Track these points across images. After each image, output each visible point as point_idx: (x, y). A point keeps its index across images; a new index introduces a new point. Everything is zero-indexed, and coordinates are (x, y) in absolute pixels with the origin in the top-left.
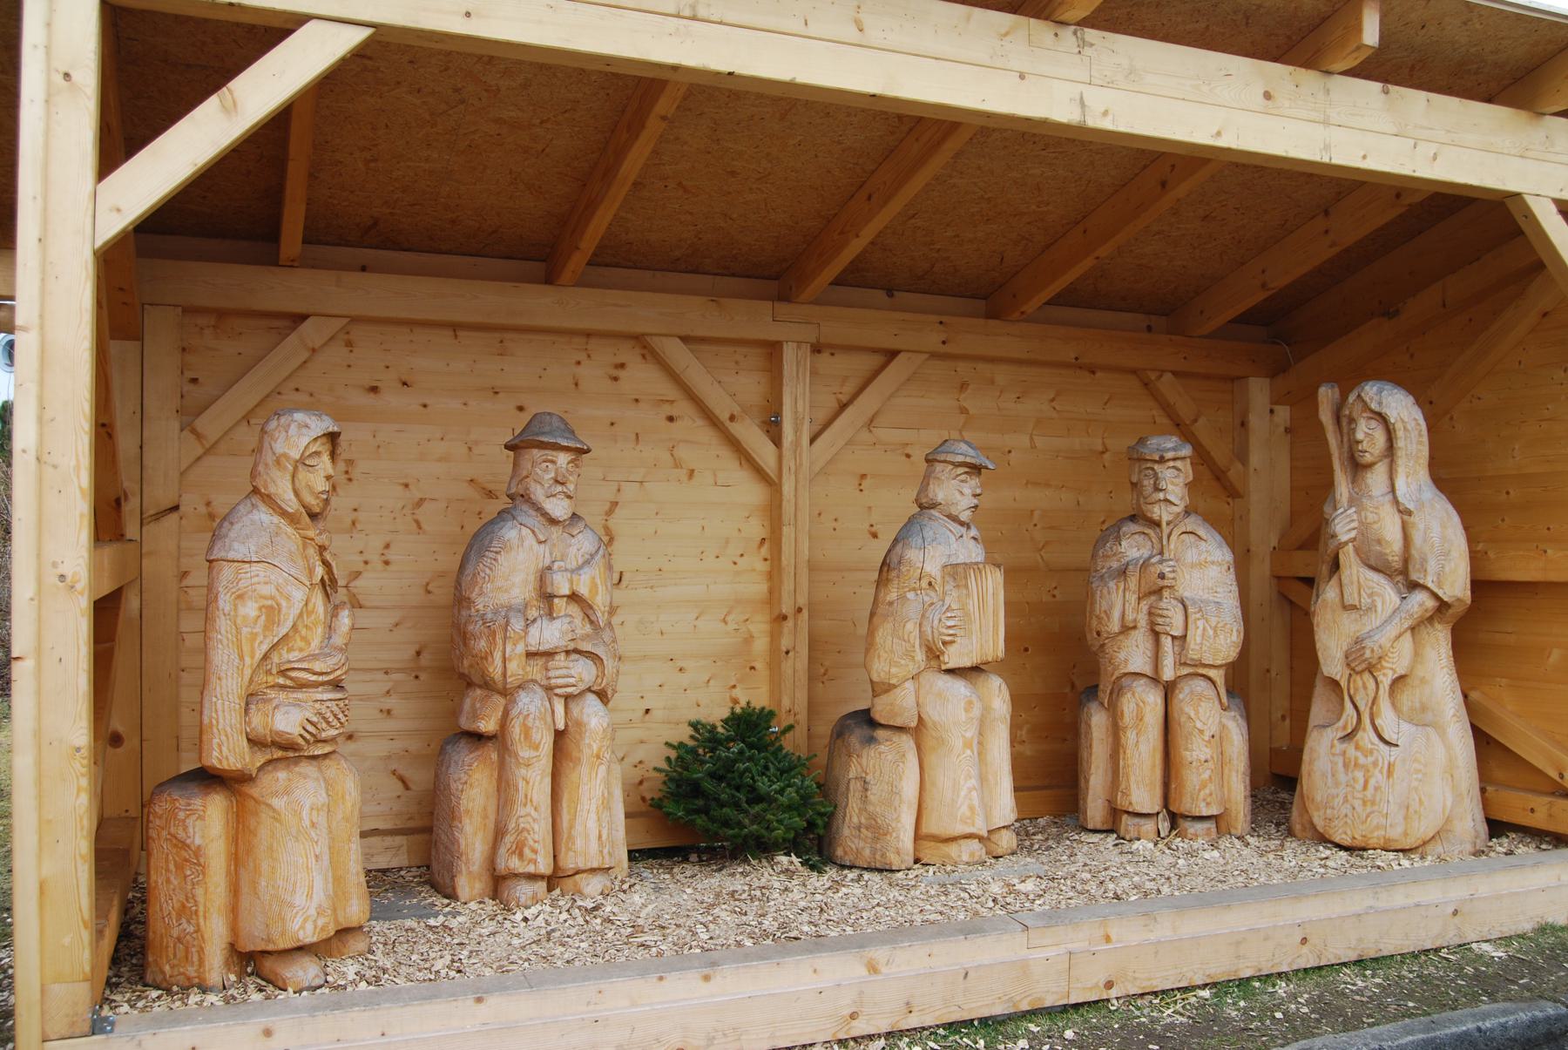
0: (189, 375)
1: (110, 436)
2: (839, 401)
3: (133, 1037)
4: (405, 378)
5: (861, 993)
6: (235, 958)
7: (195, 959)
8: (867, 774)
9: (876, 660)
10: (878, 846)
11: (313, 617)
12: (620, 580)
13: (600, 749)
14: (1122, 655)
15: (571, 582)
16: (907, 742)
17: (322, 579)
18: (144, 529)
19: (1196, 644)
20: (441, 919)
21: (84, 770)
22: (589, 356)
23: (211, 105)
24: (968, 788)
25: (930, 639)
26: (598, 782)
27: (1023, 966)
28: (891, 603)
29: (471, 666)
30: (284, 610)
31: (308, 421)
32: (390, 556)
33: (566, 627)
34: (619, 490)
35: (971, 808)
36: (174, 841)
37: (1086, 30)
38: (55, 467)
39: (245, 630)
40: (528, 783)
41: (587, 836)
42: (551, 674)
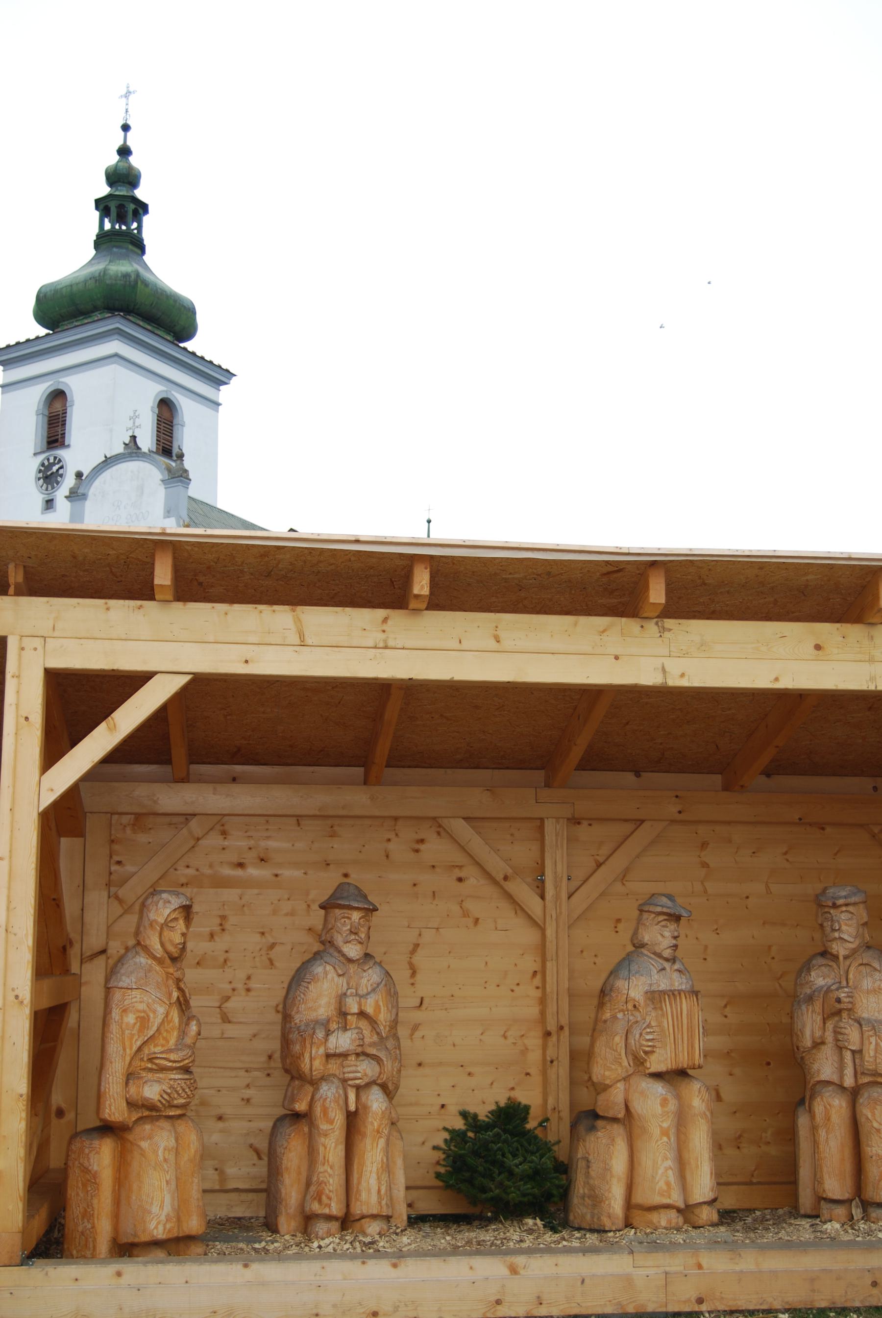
0: (116, 858)
1: (58, 906)
2: (596, 861)
3: (43, 1269)
4: (262, 855)
5: (503, 1286)
6: (116, 1249)
7: (91, 1246)
8: (589, 1154)
9: (595, 1065)
10: (596, 1211)
11: (171, 1024)
12: (421, 1003)
13: (379, 1126)
14: (815, 1067)
15: (360, 1004)
16: (618, 1130)
17: (178, 998)
18: (84, 966)
19: (870, 1057)
20: (263, 1244)
21: (24, 1108)
22: (397, 835)
23: (102, 727)
24: (665, 1167)
25: (634, 1048)
26: (379, 1150)
27: (628, 1280)
28: (605, 1021)
29: (291, 1064)
30: (152, 1020)
31: (170, 899)
32: (253, 984)
33: (354, 1036)
34: (420, 935)
35: (668, 1184)
36: (82, 1168)
37: (665, 620)
38: (15, 935)
39: (127, 1032)
40: (326, 1148)
41: (369, 1191)
42: (346, 1070)
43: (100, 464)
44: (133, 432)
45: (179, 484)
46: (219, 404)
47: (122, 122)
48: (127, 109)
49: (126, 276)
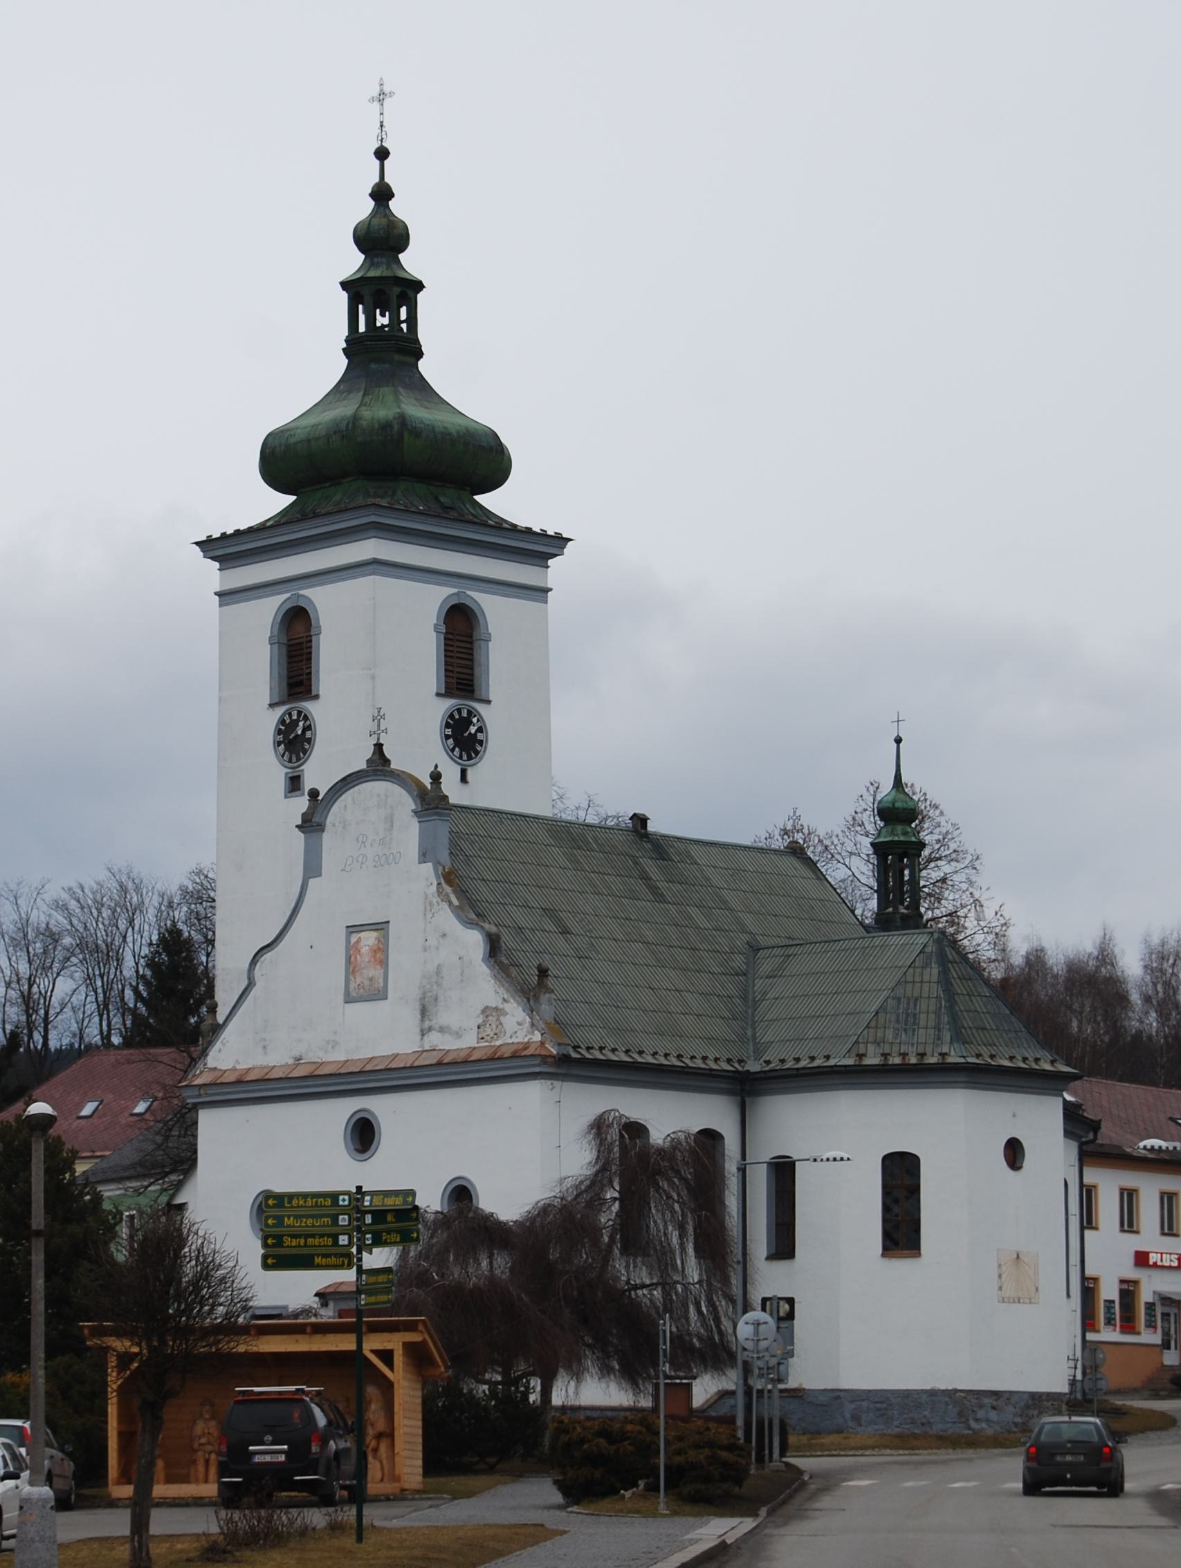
43: (337, 783)
44: (378, 739)
45: (436, 817)
46: (547, 590)
47: (377, 145)
48: (382, 122)
49: (386, 426)
